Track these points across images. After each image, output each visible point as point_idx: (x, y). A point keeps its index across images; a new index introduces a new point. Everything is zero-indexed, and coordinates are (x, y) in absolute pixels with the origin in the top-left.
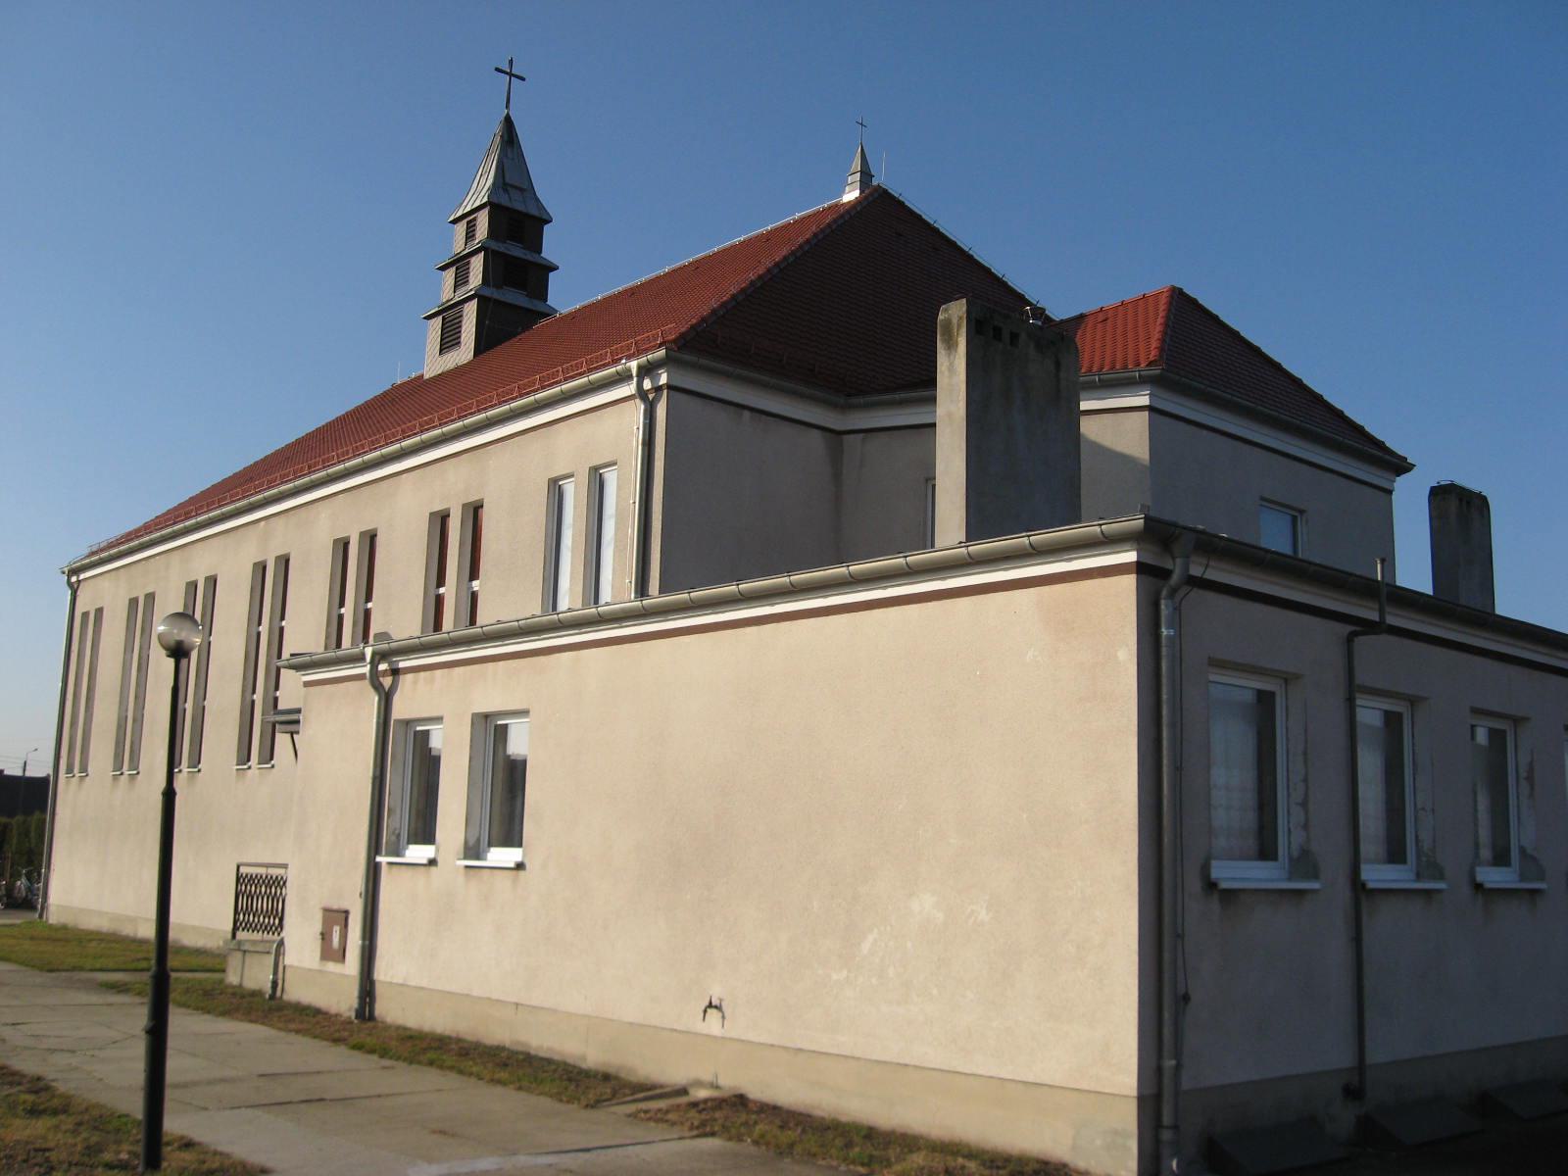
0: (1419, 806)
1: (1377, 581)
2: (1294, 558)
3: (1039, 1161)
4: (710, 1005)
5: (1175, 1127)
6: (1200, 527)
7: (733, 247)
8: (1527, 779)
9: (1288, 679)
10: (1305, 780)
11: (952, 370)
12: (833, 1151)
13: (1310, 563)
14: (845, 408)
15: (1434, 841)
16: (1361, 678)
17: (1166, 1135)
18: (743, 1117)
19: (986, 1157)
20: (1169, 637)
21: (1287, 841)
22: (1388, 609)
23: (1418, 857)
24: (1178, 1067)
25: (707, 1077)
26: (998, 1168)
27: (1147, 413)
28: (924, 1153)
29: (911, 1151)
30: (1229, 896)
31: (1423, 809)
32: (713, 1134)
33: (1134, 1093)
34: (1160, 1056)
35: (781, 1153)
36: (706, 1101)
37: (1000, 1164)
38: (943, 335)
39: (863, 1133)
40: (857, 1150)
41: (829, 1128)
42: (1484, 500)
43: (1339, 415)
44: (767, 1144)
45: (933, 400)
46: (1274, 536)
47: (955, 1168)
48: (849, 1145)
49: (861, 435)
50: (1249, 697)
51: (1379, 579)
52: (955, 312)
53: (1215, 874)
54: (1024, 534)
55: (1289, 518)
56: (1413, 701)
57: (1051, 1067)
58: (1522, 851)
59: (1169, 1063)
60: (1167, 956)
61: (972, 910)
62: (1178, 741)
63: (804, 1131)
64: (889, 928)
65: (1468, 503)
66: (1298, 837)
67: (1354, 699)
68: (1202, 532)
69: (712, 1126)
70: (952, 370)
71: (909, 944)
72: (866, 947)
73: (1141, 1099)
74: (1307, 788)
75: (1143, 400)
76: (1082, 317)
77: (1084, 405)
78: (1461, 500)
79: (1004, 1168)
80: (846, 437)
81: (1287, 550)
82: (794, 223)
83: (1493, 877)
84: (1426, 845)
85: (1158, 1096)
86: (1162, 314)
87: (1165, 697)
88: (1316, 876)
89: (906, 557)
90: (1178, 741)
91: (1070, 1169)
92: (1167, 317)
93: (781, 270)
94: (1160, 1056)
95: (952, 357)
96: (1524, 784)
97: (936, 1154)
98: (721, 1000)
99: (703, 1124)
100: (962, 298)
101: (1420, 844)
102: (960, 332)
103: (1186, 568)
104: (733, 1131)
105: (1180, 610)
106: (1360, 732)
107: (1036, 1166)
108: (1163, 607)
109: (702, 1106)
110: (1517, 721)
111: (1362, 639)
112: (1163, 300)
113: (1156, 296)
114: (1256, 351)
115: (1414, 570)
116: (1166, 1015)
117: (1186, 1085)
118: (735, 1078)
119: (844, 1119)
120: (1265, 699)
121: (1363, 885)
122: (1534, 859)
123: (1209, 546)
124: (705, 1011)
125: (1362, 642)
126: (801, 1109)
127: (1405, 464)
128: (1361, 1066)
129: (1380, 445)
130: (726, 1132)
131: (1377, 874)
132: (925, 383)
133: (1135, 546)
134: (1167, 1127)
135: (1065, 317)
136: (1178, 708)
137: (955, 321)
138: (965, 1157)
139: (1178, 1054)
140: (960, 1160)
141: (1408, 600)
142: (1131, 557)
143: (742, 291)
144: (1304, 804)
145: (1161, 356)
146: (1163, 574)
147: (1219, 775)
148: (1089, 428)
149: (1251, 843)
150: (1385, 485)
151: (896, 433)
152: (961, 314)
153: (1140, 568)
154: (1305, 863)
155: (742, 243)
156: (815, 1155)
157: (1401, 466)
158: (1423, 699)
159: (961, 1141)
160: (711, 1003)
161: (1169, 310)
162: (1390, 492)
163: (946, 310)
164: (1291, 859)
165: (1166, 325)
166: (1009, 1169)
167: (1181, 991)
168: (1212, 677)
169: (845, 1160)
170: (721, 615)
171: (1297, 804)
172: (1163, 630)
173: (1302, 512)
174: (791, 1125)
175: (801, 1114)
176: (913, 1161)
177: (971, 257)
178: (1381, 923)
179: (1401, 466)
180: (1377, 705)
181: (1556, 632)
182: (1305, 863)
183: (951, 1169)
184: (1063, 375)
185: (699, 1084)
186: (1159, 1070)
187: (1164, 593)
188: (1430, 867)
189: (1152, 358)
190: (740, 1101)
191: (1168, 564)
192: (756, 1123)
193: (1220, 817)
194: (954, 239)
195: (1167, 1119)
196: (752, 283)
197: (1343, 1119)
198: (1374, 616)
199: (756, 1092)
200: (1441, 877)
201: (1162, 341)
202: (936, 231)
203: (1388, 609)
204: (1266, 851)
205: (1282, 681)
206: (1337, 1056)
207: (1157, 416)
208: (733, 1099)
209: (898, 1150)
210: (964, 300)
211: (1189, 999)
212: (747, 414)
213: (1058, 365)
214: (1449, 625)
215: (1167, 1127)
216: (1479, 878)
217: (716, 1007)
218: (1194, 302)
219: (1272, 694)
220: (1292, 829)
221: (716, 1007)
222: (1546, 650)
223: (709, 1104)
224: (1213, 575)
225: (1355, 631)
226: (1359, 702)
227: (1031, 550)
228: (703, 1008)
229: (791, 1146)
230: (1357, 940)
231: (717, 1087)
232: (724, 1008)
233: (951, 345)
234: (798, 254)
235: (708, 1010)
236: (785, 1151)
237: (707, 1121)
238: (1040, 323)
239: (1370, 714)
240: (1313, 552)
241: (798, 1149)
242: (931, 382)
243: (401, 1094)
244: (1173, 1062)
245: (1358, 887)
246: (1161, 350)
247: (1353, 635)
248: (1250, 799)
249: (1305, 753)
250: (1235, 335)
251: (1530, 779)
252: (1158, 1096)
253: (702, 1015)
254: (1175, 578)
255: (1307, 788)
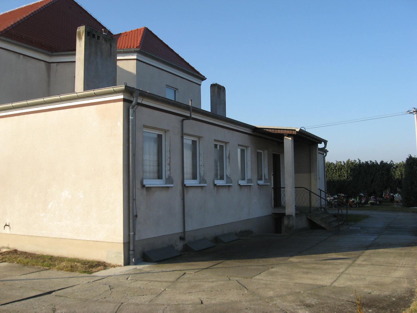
0: (200, 165)
1: (190, 106)
2: (175, 101)
3: (97, 262)
4: (6, 225)
5: (134, 250)
6: (141, 89)
7: (22, 9)
8: (228, 158)
9: (166, 131)
10: (170, 158)
11: (80, 45)
12: (40, 263)
13: (160, 97)
14: (51, 56)
15: (204, 174)
16: (185, 131)
17: (131, 252)
18: (15, 256)
19: (83, 262)
20: (131, 119)
21: (165, 174)
22: (192, 113)
23: (200, 178)
24: (134, 234)
25: (6, 245)
26: (86, 264)
27: (136, 61)
28: (66, 262)
29: (62, 262)
30: (148, 189)
31: (201, 165)
32: (5, 261)
33: (123, 242)
34: (129, 232)
35: (25, 265)
36: (5, 252)
37: (86, 263)
38: (78, 36)
39: (49, 258)
40: (46, 263)
41: (40, 257)
42: (224, 88)
43: (188, 64)
44: (21, 263)
45: (75, 54)
46: (170, 95)
47: (73, 265)
48: (44, 262)
49: (56, 64)
50: (156, 136)
51: (190, 105)
52: (82, 29)
53: (144, 183)
54: (92, 90)
55: (174, 91)
56: (199, 138)
57: (101, 237)
58: (227, 176)
59: (132, 233)
60: (131, 205)
61: (79, 195)
62: (134, 147)
63: (32, 259)
64: (56, 201)
65: (220, 89)
66: (168, 173)
67: (183, 137)
68: (142, 91)
69: (5, 259)
70: (80, 45)
71: (62, 205)
72: (49, 206)
73: (124, 243)
74: (170, 160)
75: (135, 57)
76: (121, 34)
77: (118, 58)
78: (218, 88)
79: (88, 264)
80: (51, 64)
81: (173, 99)
82: (40, 2)
83: (219, 182)
84: (202, 174)
85: (129, 243)
86: (141, 34)
87: (130, 135)
88: (172, 183)
89: (60, 96)
90: (134, 147)
91: (106, 263)
92: (143, 35)
93: (34, 15)
94: (129, 232)
95: (80, 42)
96: (227, 159)
97: (69, 262)
98: (9, 223)
99: (3, 259)
100: (84, 25)
101: (201, 174)
102: (83, 35)
103: (137, 100)
104: (11, 260)
105: (135, 112)
106: (184, 145)
107: (96, 263)
108: (130, 111)
109: (3, 254)
110: (226, 143)
111: (185, 121)
112: (142, 30)
113: (141, 29)
114: (167, 46)
115: (206, 105)
116: (131, 221)
117: (137, 239)
118: (13, 246)
119: (45, 254)
120: (160, 136)
121: (185, 185)
122: (229, 178)
123: (143, 94)
124: (4, 227)
125: (185, 122)
126: (33, 252)
127: (204, 78)
128: (184, 232)
129: (198, 73)
130: (11, 261)
131: (188, 182)
132: (72, 49)
133: (123, 93)
134: (131, 250)
135: (116, 34)
136: (134, 138)
137: (82, 32)
138: (77, 262)
139: (134, 231)
140: (76, 263)
141: (204, 113)
142: (121, 97)
143: (21, 20)
144: (169, 164)
145: (140, 45)
146: (130, 102)
147: (147, 157)
148: (119, 64)
149: (156, 175)
150: (199, 83)
151: (66, 63)
152: (83, 30)
153: (124, 100)
154: (170, 180)
155: (25, 7)
156: (34, 265)
157: (203, 78)
158: (202, 137)
159: (77, 258)
160: (6, 224)
161: (143, 33)
162: (200, 85)
163: (79, 29)
164: (166, 179)
165: (142, 37)
166: (88, 265)
167: (135, 214)
168: (144, 130)
169: (43, 266)
170: (7, 113)
171: (168, 164)
172: (130, 117)
173: (177, 89)
174: (29, 257)
175: (33, 254)
176: (62, 265)
177: (91, 16)
178: (189, 195)
179: (203, 78)
180: (190, 139)
181: (250, 125)
182: (170, 180)
183: (72, 266)
184: (112, 49)
185: (4, 247)
186: (129, 235)
187: (131, 107)
188: (203, 180)
189: (137, 46)
190: (16, 251)
191: (132, 99)
192: (18, 257)
193: (147, 168)
194: (86, 10)
195: (131, 248)
196: (24, 18)
197: (180, 245)
198: (189, 115)
199: (20, 249)
200: (206, 183)
201: (141, 41)
202: (81, 8)
203: (192, 113)
204: (160, 177)
205: (164, 132)
206: (178, 229)
207: (138, 62)
208: (13, 251)
209: (58, 262)
210: (84, 26)
211: (137, 216)
212: (21, 56)
213: (111, 46)
214: (198, 115)
215: (131, 250)
216: (215, 183)
217: (8, 225)
218: (151, 32)
219: (161, 135)
220: (166, 171)
221: (8, 225)
222: (234, 125)
223: (6, 253)
224: (144, 102)
225: (184, 119)
226: (184, 138)
227: (94, 95)
228: (4, 226)
229: (28, 263)
230: (183, 199)
231: (9, 248)
232: (10, 226)
233: (80, 39)
234: (39, 11)
235: (5, 226)
236: (26, 264)
237: (3, 258)
238: (106, 34)
239: (188, 141)
240: (180, 99)
241: (30, 263)
242: (75, 50)
243: (54, 291)
244: (133, 233)
245: (184, 186)
246: (140, 44)
247: (183, 120)
248: (156, 164)
249: (170, 151)
250: (161, 41)
251: (229, 158)
252: (129, 243)
253: (4, 228)
254: (134, 103)
255: (170, 160)
